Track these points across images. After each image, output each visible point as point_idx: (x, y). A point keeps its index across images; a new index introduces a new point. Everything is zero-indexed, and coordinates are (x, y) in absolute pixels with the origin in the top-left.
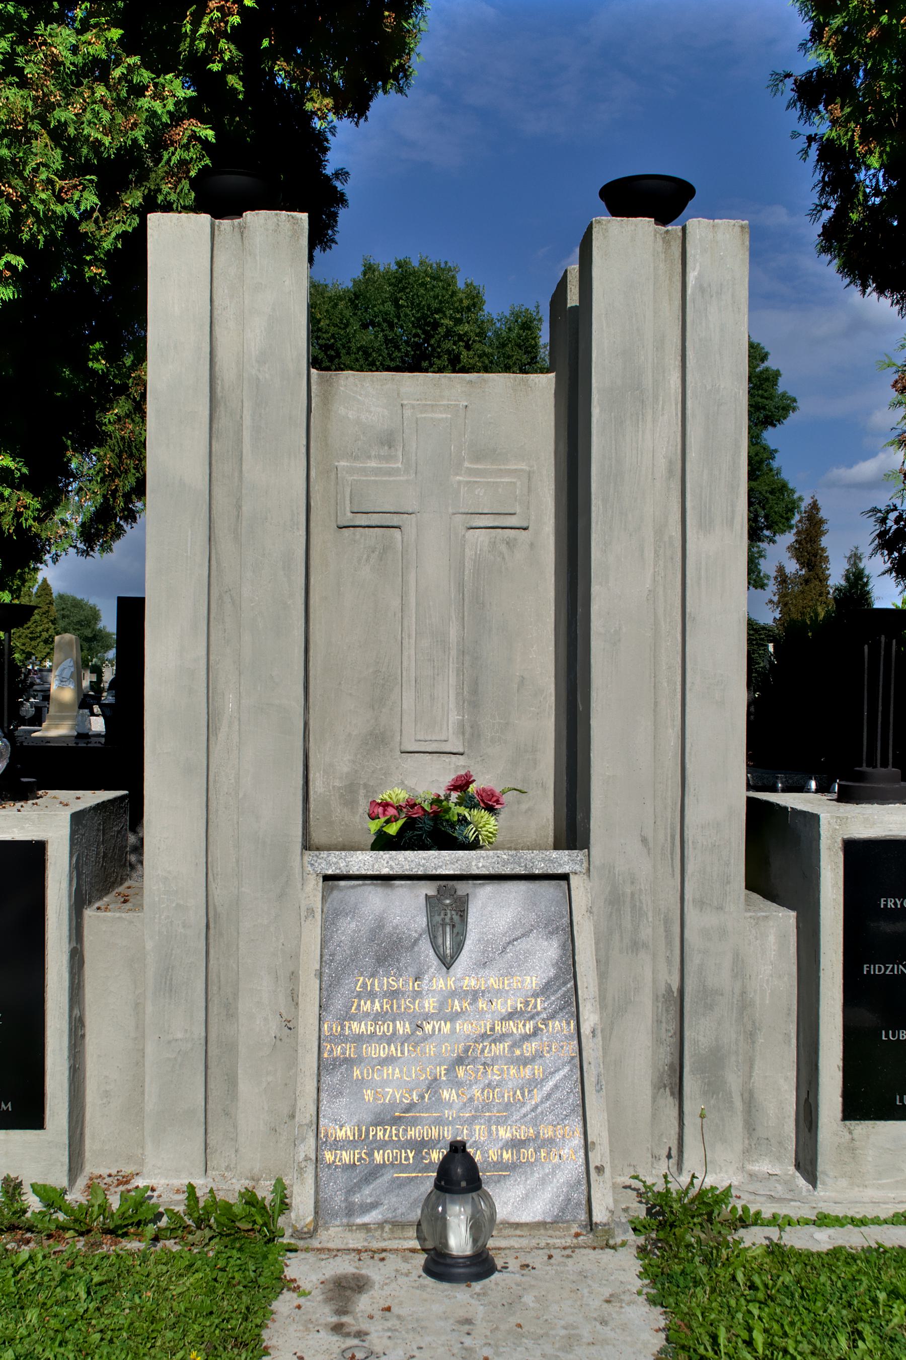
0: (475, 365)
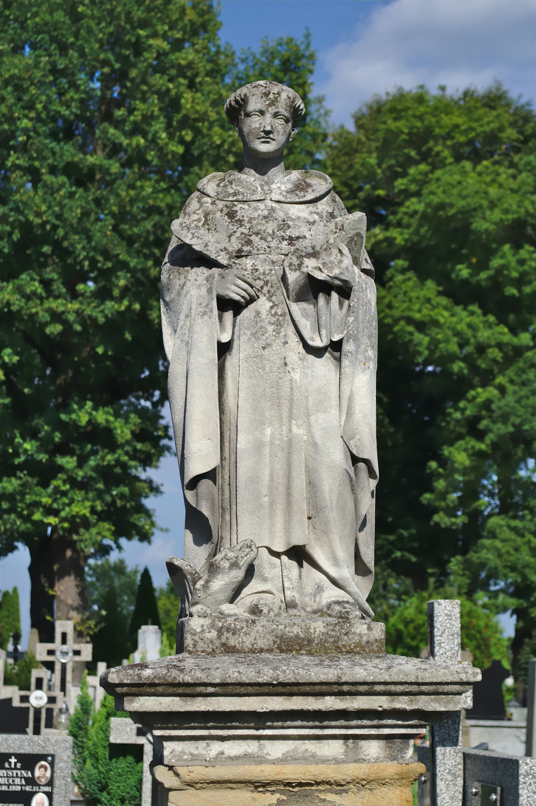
0: (205, 113)
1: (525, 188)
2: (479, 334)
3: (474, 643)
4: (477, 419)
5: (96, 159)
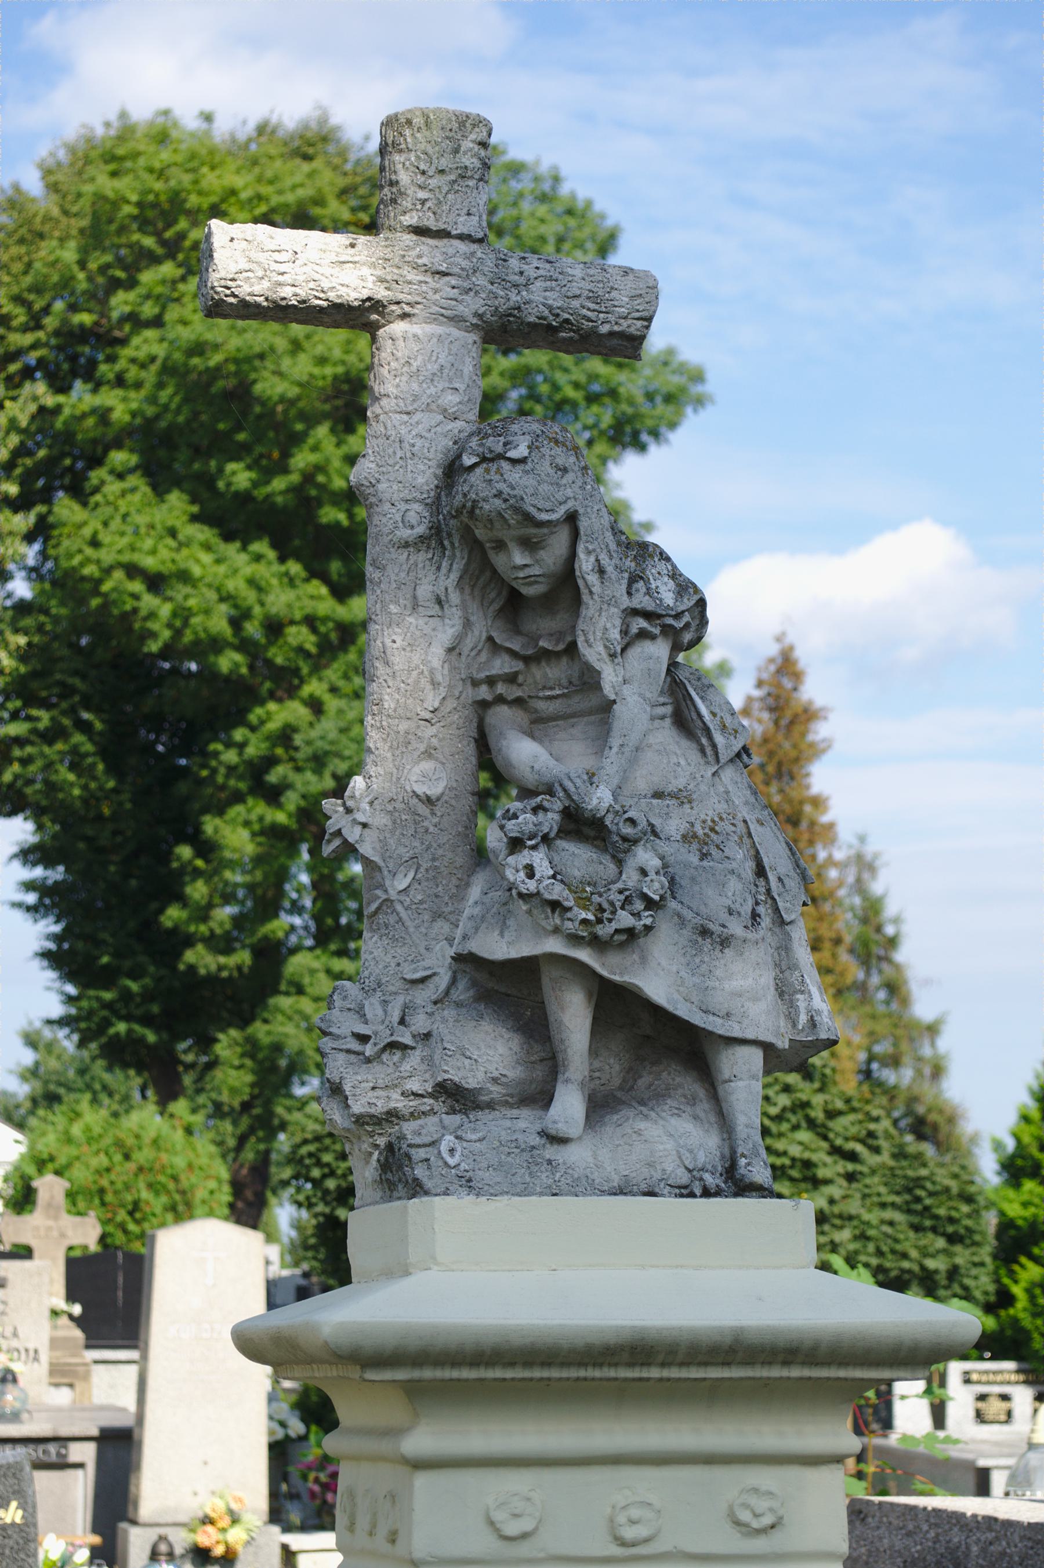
2: (270, 599)
3: (164, 1199)
4: (270, 761)
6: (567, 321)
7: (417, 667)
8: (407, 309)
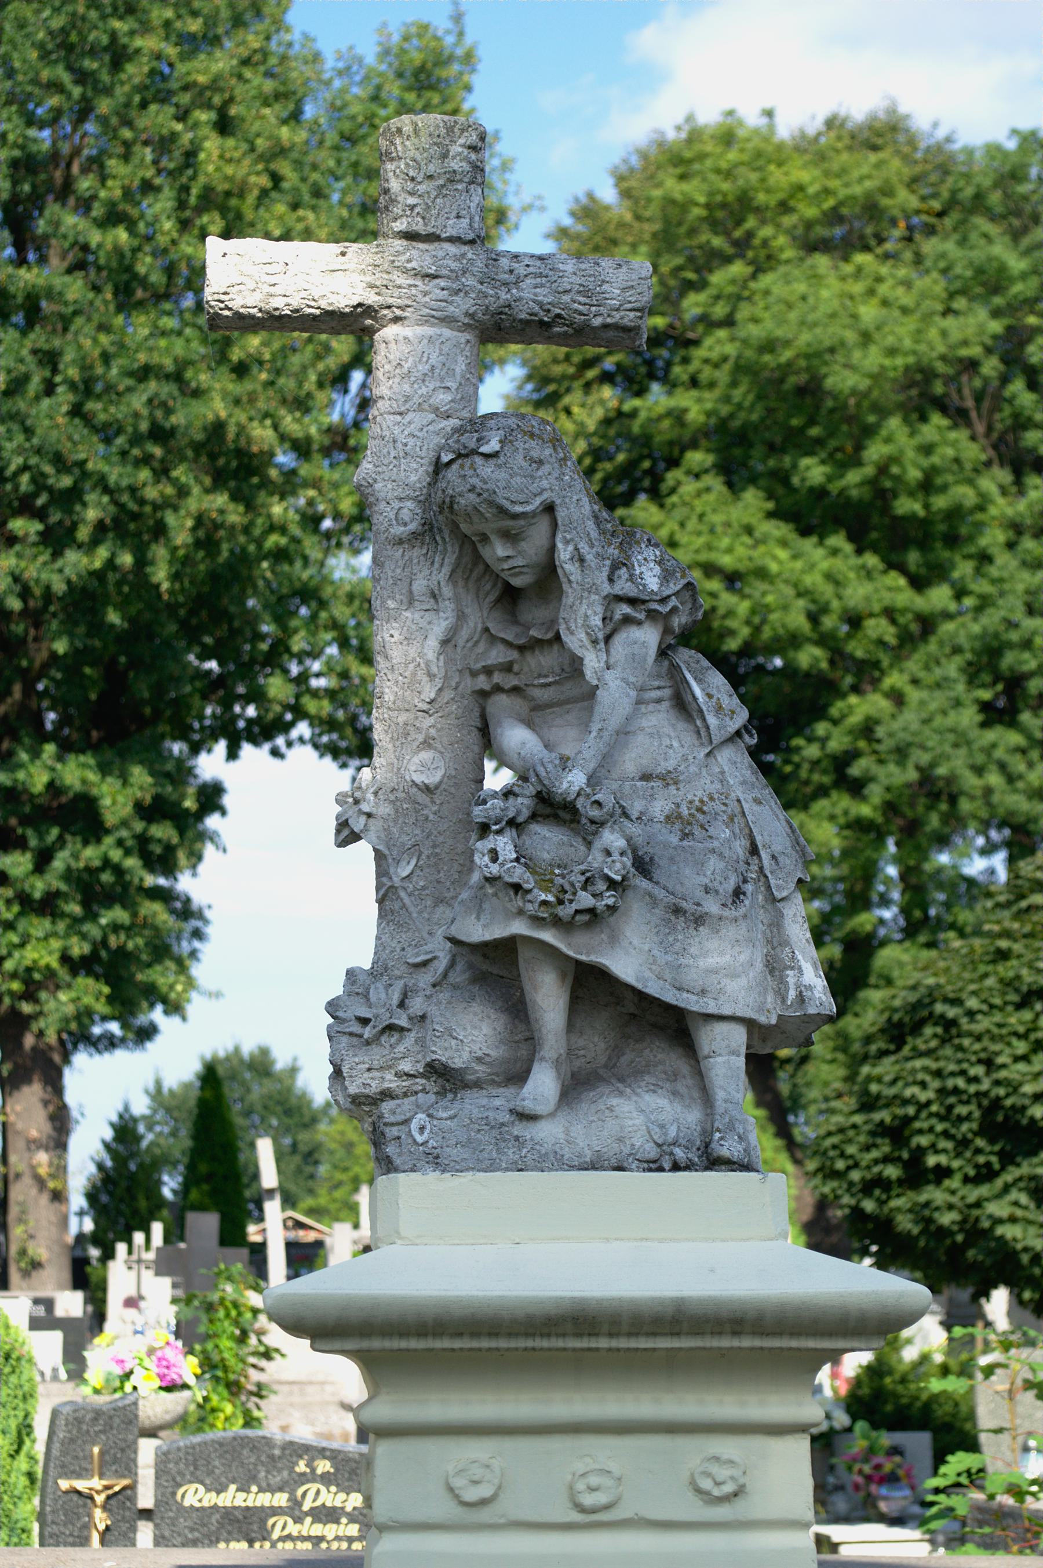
1: (928, 305)
2: (848, 592)
4: (851, 756)
5: (38, 276)
6: (559, 316)
7: (413, 660)
8: (398, 312)
